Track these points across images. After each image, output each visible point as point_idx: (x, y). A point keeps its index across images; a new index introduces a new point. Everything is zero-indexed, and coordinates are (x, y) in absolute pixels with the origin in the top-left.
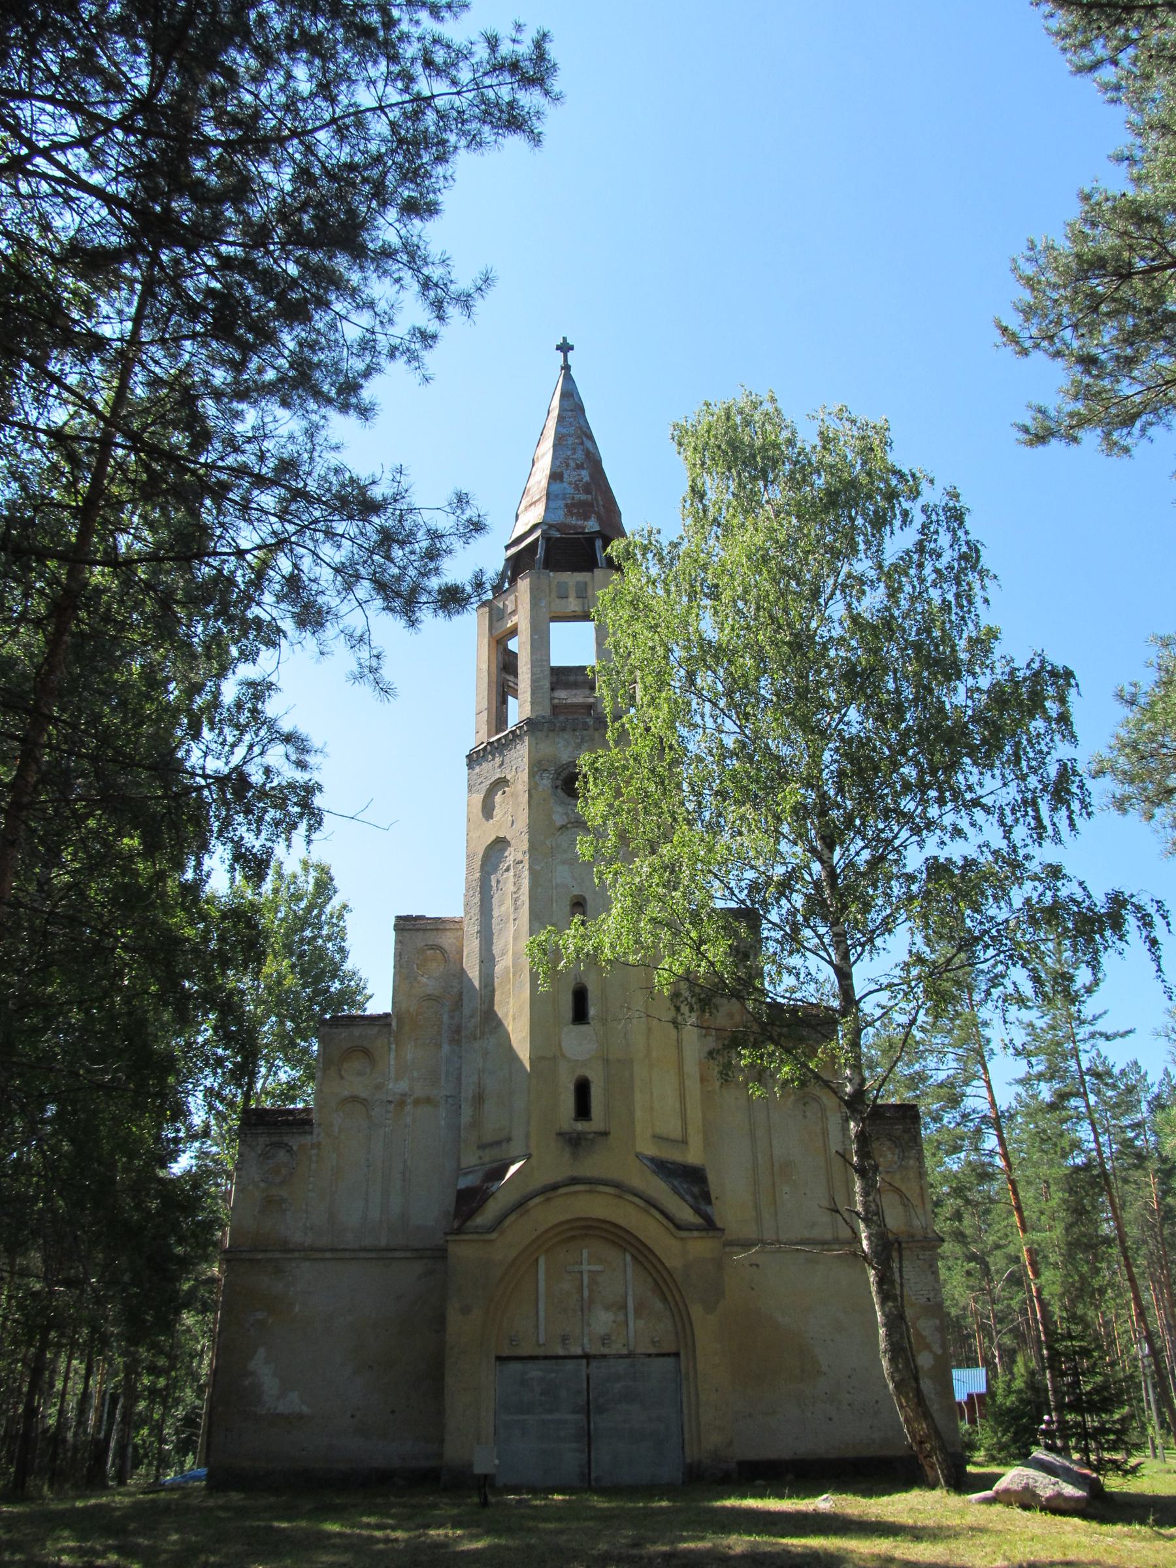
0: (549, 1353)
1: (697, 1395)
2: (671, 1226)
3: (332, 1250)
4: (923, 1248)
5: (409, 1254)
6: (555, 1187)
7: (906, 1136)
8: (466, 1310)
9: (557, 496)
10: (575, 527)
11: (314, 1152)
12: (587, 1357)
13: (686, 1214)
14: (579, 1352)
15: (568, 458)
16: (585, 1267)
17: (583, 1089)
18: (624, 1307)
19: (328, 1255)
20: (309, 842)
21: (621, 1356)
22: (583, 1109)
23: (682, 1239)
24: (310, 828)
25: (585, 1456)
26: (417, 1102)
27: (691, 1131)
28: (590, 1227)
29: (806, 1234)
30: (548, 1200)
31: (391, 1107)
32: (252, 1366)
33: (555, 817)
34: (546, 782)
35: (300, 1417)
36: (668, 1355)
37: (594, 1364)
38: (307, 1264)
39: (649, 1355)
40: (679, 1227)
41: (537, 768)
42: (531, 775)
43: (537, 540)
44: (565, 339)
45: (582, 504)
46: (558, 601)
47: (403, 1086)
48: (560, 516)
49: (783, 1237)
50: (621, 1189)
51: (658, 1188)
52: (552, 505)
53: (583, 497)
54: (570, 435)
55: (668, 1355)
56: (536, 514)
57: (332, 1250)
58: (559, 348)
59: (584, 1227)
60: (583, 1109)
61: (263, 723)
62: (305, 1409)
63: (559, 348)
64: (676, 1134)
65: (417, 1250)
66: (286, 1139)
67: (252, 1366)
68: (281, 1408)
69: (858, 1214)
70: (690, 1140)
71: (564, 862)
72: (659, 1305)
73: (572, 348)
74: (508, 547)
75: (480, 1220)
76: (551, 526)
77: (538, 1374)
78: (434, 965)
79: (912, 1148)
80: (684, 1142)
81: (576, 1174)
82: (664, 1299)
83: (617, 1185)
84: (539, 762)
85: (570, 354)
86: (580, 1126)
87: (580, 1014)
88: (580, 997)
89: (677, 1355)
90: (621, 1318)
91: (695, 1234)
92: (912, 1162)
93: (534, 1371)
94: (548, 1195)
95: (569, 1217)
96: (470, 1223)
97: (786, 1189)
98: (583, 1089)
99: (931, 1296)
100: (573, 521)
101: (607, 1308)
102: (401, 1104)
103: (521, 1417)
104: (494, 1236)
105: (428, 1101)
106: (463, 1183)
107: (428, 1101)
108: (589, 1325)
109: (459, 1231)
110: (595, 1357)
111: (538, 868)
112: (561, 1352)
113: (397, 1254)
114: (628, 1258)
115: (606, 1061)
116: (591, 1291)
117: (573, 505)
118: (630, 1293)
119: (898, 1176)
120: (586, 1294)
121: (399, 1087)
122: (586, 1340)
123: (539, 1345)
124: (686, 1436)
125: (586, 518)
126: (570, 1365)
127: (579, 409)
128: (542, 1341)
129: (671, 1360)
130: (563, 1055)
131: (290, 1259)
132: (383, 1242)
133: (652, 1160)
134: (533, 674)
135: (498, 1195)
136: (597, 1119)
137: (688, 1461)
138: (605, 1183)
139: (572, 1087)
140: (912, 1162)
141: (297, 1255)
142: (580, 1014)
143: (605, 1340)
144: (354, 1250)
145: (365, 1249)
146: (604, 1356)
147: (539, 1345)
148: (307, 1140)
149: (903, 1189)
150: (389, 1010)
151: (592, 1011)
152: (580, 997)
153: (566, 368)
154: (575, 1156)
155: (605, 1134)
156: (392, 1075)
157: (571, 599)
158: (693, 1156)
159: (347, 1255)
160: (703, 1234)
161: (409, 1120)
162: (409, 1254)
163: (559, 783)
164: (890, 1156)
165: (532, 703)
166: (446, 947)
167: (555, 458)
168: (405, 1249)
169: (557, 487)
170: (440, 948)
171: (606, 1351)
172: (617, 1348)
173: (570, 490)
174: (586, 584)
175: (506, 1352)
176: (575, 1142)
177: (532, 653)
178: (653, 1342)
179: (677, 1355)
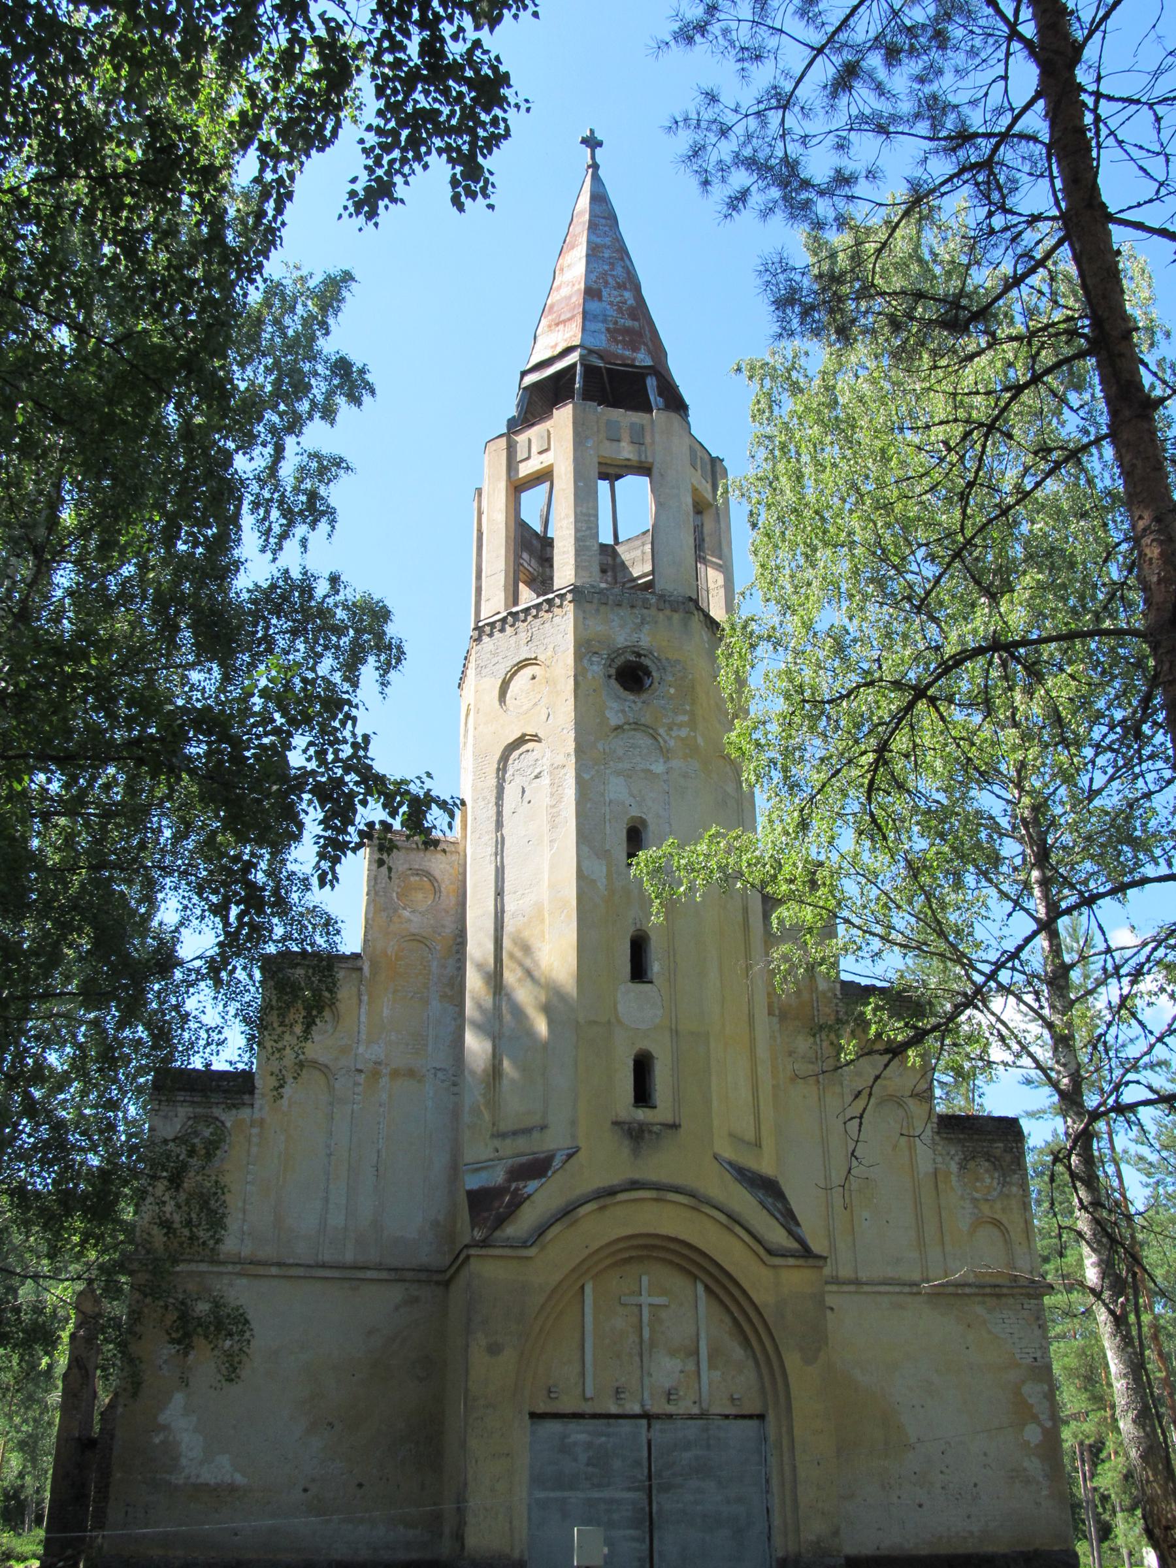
0: (598, 1411)
1: (794, 1468)
2: (762, 1252)
3: (279, 1264)
4: (1029, 1296)
5: (384, 1275)
6: (611, 1192)
7: (1008, 1158)
8: (494, 1349)
9: (595, 317)
10: (622, 357)
11: (255, 1131)
12: (647, 1416)
13: (777, 1236)
14: (637, 1409)
15: (605, 273)
16: (645, 1299)
17: (643, 1067)
18: (697, 1353)
19: (274, 1270)
20: (384, 684)
21: (691, 1417)
22: (643, 1095)
23: (774, 1267)
24: (385, 669)
25: (646, 1546)
26: (395, 1074)
27: (765, 1133)
28: (654, 1247)
29: (890, 1272)
30: (602, 1208)
31: (361, 1078)
32: (162, 1419)
33: (608, 714)
34: (597, 669)
35: (232, 1488)
36: (750, 1417)
37: (657, 1425)
38: (244, 1281)
39: (727, 1417)
40: (770, 1252)
41: (584, 649)
42: (579, 657)
43: (574, 366)
44: (592, 131)
45: (627, 331)
46: (607, 443)
47: (376, 1052)
48: (601, 342)
49: (863, 1276)
50: (697, 1200)
51: (743, 1201)
52: (589, 325)
53: (629, 323)
54: (604, 246)
55: (750, 1417)
56: (571, 334)
57: (279, 1264)
58: (585, 141)
59: (645, 1247)
60: (643, 1095)
61: (323, 513)
62: (239, 1479)
63: (585, 141)
64: (750, 1135)
65: (396, 1270)
66: (217, 1112)
67: (162, 1419)
68: (207, 1476)
69: (1080, 1234)
70: (764, 1143)
71: (618, 773)
72: (738, 1353)
73: (600, 144)
74: (524, 374)
75: (511, 1230)
76: (591, 352)
77: (583, 1437)
78: (420, 896)
79: (1014, 1172)
80: (758, 1145)
81: (637, 1176)
82: (746, 1342)
83: (692, 1195)
84: (588, 641)
85: (598, 151)
86: (642, 1114)
87: (639, 972)
88: (639, 947)
89: (761, 1417)
90: (691, 1366)
91: (791, 1261)
92: (1014, 1189)
93: (578, 1434)
94: (602, 1202)
95: (629, 1231)
96: (498, 1234)
97: (866, 1214)
98: (643, 1067)
99: (1038, 1355)
100: (619, 350)
101: (673, 1353)
102: (375, 1075)
103: (558, 1494)
104: (532, 1252)
105: (411, 1073)
106: (473, 1182)
107: (411, 1073)
108: (650, 1375)
109: (484, 1243)
110: (658, 1417)
111: (587, 777)
112: (614, 1409)
113: (369, 1274)
114: (700, 1288)
115: (675, 1033)
116: (652, 1331)
117: (616, 331)
118: (703, 1335)
119: (998, 1206)
120: (646, 1334)
121: (368, 1053)
122: (646, 1395)
123: (586, 1399)
124: (777, 1521)
125: (635, 349)
126: (626, 1427)
127: (612, 219)
128: (589, 1394)
129: (754, 1423)
130: (619, 1022)
131: (221, 1273)
132: (349, 1257)
133: (730, 1163)
134: (577, 530)
135: (537, 1198)
136: (663, 1109)
137: (780, 1554)
138: (677, 1190)
139: (631, 1064)
140: (1014, 1189)
141: (230, 1268)
142: (639, 972)
143: (669, 1395)
144: (309, 1266)
145: (323, 1266)
146: (670, 1416)
147: (586, 1399)
148: (245, 1114)
149: (1005, 1221)
150: (358, 950)
151: (656, 967)
152: (639, 947)
153: (595, 166)
154: (636, 1152)
155: (675, 1126)
156: (363, 1037)
157: (623, 444)
158: (766, 1166)
159: (300, 1272)
160: (801, 1262)
161: (384, 1096)
162: (384, 1275)
163: (613, 671)
164: (988, 1180)
165: (577, 567)
166: (437, 873)
167: (589, 271)
168: (379, 1267)
169: (595, 306)
170: (428, 874)
171: (670, 1409)
172: (686, 1406)
173: (611, 312)
174: (642, 427)
175: (541, 1408)
176: (636, 1135)
177: (576, 505)
178: (732, 1399)
179: (761, 1417)
